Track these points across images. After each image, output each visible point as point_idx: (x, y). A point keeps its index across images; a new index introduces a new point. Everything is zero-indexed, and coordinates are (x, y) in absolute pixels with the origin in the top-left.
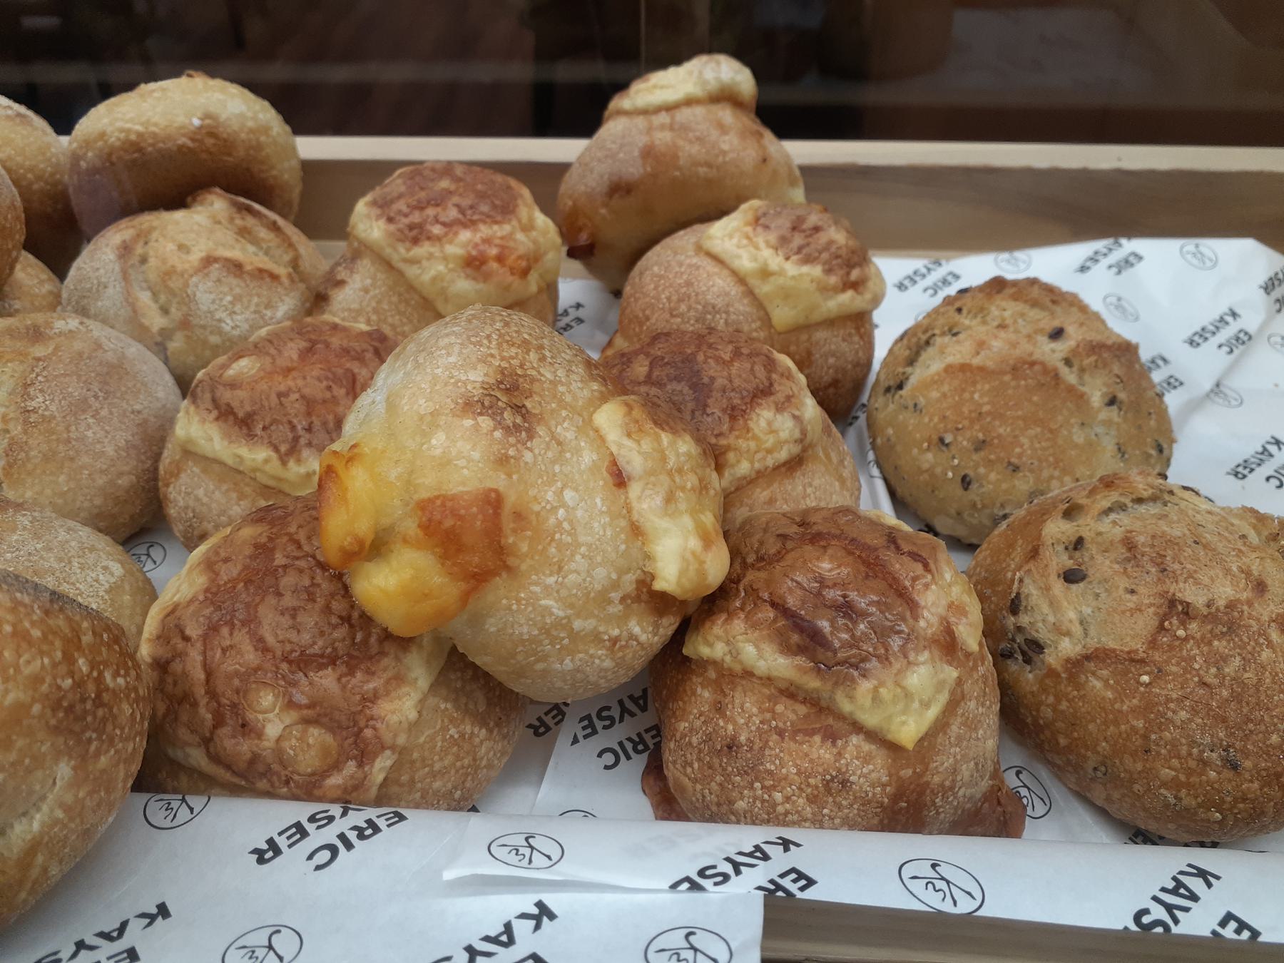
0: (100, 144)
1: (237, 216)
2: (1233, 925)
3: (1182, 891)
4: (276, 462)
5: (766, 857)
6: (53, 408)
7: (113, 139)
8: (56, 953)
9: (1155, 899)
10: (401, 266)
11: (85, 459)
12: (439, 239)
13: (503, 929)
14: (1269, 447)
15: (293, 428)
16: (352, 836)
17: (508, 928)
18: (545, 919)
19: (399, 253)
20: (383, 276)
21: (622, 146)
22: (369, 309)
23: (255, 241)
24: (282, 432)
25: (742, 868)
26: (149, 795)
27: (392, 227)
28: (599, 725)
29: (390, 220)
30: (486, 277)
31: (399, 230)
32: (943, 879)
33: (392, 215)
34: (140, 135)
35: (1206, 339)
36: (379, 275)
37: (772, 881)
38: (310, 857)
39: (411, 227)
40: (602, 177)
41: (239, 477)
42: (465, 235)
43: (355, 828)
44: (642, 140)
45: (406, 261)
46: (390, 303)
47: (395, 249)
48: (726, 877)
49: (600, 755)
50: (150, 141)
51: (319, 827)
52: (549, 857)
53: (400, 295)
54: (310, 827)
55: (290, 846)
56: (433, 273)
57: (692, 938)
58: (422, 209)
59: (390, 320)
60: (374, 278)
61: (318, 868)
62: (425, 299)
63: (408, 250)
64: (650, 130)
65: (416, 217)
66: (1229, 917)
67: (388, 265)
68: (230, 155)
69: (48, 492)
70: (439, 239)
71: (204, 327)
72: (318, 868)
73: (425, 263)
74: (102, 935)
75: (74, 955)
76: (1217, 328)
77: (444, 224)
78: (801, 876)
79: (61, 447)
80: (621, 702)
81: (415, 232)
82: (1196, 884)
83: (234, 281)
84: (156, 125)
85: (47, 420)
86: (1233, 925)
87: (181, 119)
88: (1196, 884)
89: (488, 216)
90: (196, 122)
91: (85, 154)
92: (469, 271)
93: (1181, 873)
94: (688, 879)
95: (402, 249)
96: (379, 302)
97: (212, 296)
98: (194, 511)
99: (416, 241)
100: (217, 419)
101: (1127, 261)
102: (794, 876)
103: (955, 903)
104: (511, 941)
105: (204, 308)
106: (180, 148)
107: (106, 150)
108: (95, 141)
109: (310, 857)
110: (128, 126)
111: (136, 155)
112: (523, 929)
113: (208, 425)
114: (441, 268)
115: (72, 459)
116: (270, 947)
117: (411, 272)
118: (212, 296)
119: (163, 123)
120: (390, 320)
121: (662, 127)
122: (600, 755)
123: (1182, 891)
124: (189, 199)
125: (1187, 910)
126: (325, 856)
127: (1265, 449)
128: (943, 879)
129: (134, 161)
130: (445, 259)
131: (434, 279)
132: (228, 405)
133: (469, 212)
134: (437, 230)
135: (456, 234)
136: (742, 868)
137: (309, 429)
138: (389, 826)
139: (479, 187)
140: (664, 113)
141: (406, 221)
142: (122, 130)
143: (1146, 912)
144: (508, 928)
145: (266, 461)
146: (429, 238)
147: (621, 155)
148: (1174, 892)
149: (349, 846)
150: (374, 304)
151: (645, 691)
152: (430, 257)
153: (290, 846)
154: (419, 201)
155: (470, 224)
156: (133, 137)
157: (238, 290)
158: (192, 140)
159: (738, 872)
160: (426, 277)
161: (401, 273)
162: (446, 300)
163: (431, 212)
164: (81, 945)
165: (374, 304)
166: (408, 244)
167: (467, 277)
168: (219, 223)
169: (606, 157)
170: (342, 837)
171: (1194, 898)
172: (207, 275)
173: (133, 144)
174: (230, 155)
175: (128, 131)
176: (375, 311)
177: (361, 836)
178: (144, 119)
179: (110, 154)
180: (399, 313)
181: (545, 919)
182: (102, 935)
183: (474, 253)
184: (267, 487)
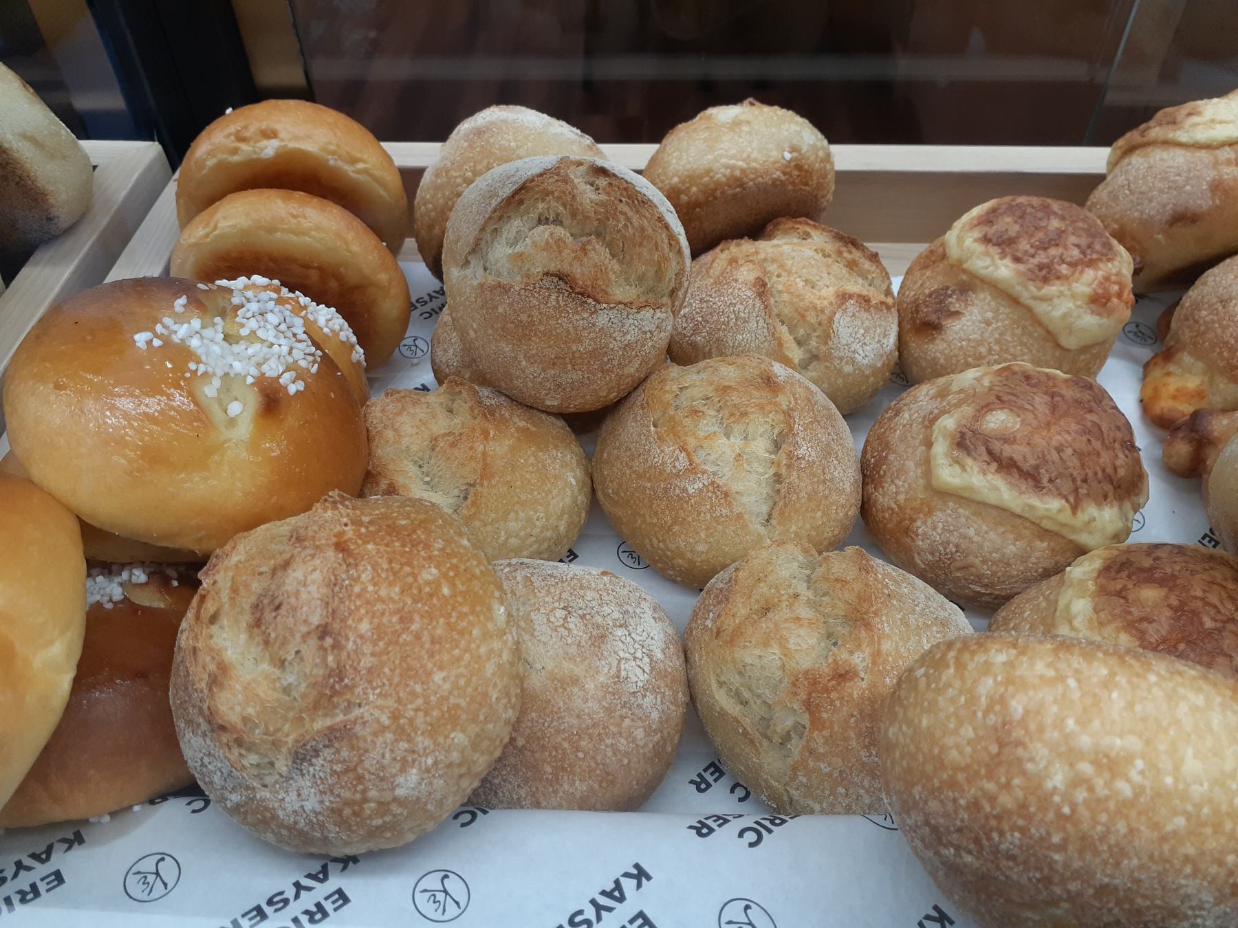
0: (706, 179)
1: (844, 249)
4: (1069, 511)
6: (813, 454)
7: (719, 176)
10: (1031, 303)
11: (834, 497)
12: (1067, 278)
13: (613, 886)
15: (1074, 480)
18: (644, 880)
19: (1028, 292)
20: (1008, 310)
21: (1188, 179)
22: (991, 340)
23: (863, 275)
24: (1067, 486)
27: (1021, 267)
29: (1017, 260)
30: (1110, 313)
31: (1029, 270)
33: (1019, 255)
34: (743, 171)
36: (1002, 309)
37: (700, 822)
39: (1041, 267)
40: (1164, 206)
41: (1019, 521)
42: (1089, 274)
43: (306, 912)
44: (1210, 175)
45: (1035, 298)
46: (1013, 334)
47: (1026, 287)
50: (752, 176)
51: (276, 910)
53: (1024, 328)
54: (268, 910)
55: (335, 910)
56: (1063, 310)
57: (446, 881)
58: (1045, 249)
59: (1012, 350)
60: (996, 312)
61: (194, 811)
62: (1048, 332)
63: (1039, 289)
64: (1216, 164)
65: (1042, 258)
67: (1015, 301)
68: (806, 184)
69: (808, 526)
70: (1067, 278)
71: (841, 359)
72: (194, 811)
73: (1056, 301)
75: (15, 875)
77: (1069, 264)
79: (821, 488)
80: (593, 902)
81: (1044, 272)
83: (865, 315)
84: (755, 160)
85: (811, 464)
87: (775, 154)
89: (1103, 255)
90: (788, 156)
91: (689, 189)
92: (1092, 306)
95: (1032, 287)
96: (1001, 334)
97: (850, 330)
98: (957, 546)
99: (1046, 280)
100: (997, 471)
104: (622, 899)
105: (844, 341)
106: (774, 181)
107: (712, 186)
108: (701, 177)
110: (733, 162)
111: (738, 190)
112: (628, 885)
113: (990, 477)
114: (1071, 305)
115: (826, 497)
116: (157, 874)
117: (1041, 308)
118: (850, 330)
119: (761, 159)
120: (1012, 350)
121: (1228, 162)
123: (617, 894)
124: (770, 227)
129: (734, 196)
130: (1074, 297)
131: (1065, 316)
132: (1011, 459)
133: (1089, 251)
134: (1064, 269)
135: (1081, 273)
137: (1085, 481)
140: (1227, 148)
141: (1036, 261)
142: (727, 167)
145: (1060, 511)
146: (1058, 278)
147: (1188, 188)
150: (997, 336)
152: (1061, 294)
153: (335, 910)
154: (1041, 241)
155: (1091, 264)
156: (738, 173)
157: (867, 323)
158: (784, 173)
159: (599, 918)
160: (1057, 314)
161: (1029, 310)
162: (1070, 333)
163: (1053, 251)
165: (997, 336)
166: (1039, 284)
167: (1092, 312)
168: (829, 256)
169: (1169, 188)
172: (845, 310)
173: (737, 179)
174: (806, 184)
175: (733, 167)
176: (998, 342)
177: (312, 920)
178: (745, 155)
179: (715, 190)
180: (1022, 344)
181: (644, 880)
183: (1100, 291)
184: (1047, 531)
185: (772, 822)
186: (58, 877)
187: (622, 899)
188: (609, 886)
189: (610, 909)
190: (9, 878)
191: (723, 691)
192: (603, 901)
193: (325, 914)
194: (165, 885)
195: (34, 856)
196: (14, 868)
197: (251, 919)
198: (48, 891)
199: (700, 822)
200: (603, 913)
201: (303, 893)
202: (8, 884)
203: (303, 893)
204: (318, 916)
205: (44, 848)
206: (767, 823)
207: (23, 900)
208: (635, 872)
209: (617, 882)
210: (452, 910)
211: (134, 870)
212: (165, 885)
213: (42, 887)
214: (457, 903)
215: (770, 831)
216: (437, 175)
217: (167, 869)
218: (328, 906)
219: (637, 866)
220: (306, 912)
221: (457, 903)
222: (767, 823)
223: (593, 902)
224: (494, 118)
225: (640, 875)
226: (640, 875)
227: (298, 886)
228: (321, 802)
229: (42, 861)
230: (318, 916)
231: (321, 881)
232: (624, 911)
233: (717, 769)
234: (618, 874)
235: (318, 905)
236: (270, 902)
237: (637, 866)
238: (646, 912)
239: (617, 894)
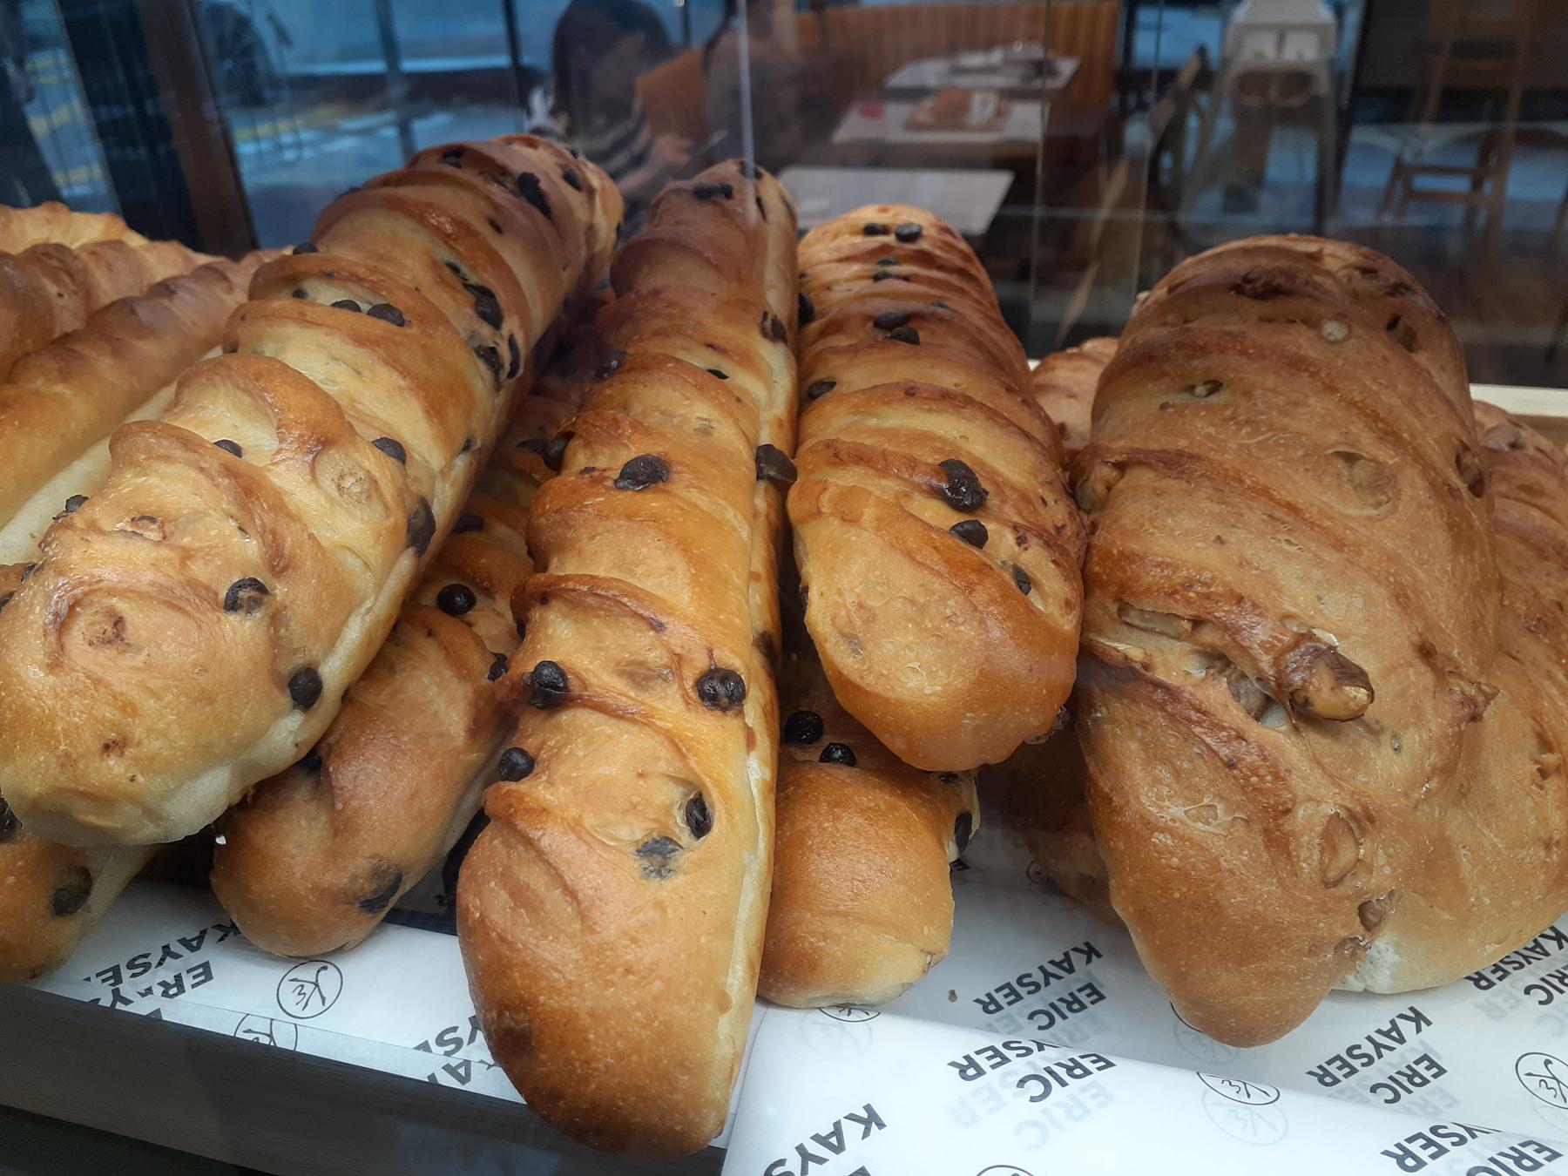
2: (1426, 1063)
3: (1394, 1034)
5: (1071, 970)
9: (1369, 1038)
17: (837, 1130)
25: (1052, 980)
26: (538, 331)
28: (1022, 991)
35: (1442, 1151)
37: (967, 1058)
49: (1017, 1131)
66: (1425, 1057)
76: (1378, 1046)
78: (1433, 1064)
80: (1042, 968)
82: (1407, 1028)
86: (1426, 1063)
88: (1407, 1028)
93: (1401, 1016)
101: (1412, 1075)
112: (852, 1131)
122: (1017, 1131)
123: (1394, 1034)
136: (1052, 980)
144: (837, 1130)
148: (1387, 1034)
151: (1066, 954)
159: (1047, 983)
171: (1401, 1040)
185: (1070, 1070)
187: (839, 1149)
189: (821, 1161)
190: (154, 964)
192: (1051, 969)
194: (323, 999)
195: (185, 943)
199: (967, 1058)
201: (168, 959)
203: (168, 959)
204: (173, 991)
206: (1062, 1072)
208: (865, 1115)
209: (837, 1125)
212: (323, 999)
213: (188, 981)
215: (1063, 1084)
216: (166, 308)
219: (868, 1108)
220: (163, 984)
222: (1062, 1072)
223: (801, 1149)
224: (1100, 349)
225: (871, 1120)
226: (871, 1120)
227: (166, 948)
229: (193, 949)
233: (1095, 991)
234: (840, 1116)
235: (178, 978)
237: (868, 1108)
239: (834, 1140)
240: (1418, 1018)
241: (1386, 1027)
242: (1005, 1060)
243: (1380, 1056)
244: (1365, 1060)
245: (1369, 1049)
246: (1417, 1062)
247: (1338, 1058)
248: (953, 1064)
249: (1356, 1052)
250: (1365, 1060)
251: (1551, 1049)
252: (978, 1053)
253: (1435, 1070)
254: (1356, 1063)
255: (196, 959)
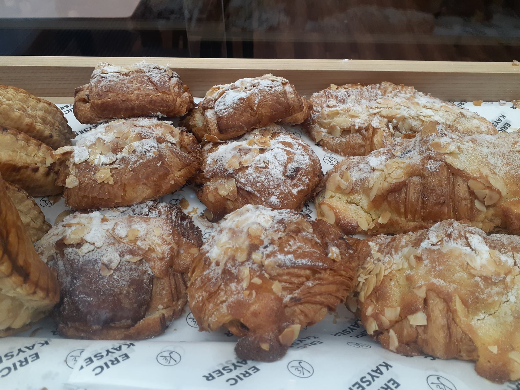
2: (392, 382)
8: (12, 352)
9: (369, 374)
14: (380, 367)
16: (109, 364)
18: (389, 367)
32: (442, 384)
37: (210, 374)
38: (94, 370)
43: (111, 361)
48: (231, 370)
51: (7, 359)
52: (176, 361)
54: (94, 359)
61: (96, 374)
66: (391, 380)
72: (96, 374)
74: (27, 347)
75: (18, 354)
78: (395, 382)
82: (383, 369)
86: (392, 382)
88: (383, 369)
93: (380, 365)
94: (219, 371)
102: (253, 369)
103: (304, 374)
109: (94, 370)
116: (171, 357)
123: (378, 371)
125: (378, 377)
126: (99, 370)
127: (378, 369)
128: (442, 384)
138: (123, 360)
139: (197, 107)
143: (364, 377)
148: (376, 371)
149: (108, 367)
164: (20, 350)
170: (106, 364)
171: (381, 373)
177: (113, 363)
181: (389, 367)
182: (27, 347)
185: (244, 375)
186: (37, 356)
188: (375, 369)
191: (483, 135)
193: (118, 361)
196: (17, 351)
197: (32, 358)
198: (32, 361)
200: (375, 378)
202: (15, 358)
205: (31, 345)
207: (21, 365)
208: (386, 387)
210: (307, 374)
211: (160, 355)
213: (30, 360)
214: (309, 372)
217: (175, 356)
218: (120, 359)
221: (309, 372)
222: (242, 376)
228: (288, 313)
230: (115, 362)
231: (118, 350)
232: (380, 381)
234: (377, 365)
236: (95, 356)
238: (394, 378)
240: (387, 366)
241: (375, 369)
242: (222, 374)
243: (374, 380)
244: (368, 383)
245: (369, 378)
246: (389, 382)
247: (357, 383)
248: (205, 376)
249: (364, 380)
250: (368, 383)
251: (440, 373)
252: (213, 372)
253: (396, 385)
254: (364, 385)
255: (32, 352)
